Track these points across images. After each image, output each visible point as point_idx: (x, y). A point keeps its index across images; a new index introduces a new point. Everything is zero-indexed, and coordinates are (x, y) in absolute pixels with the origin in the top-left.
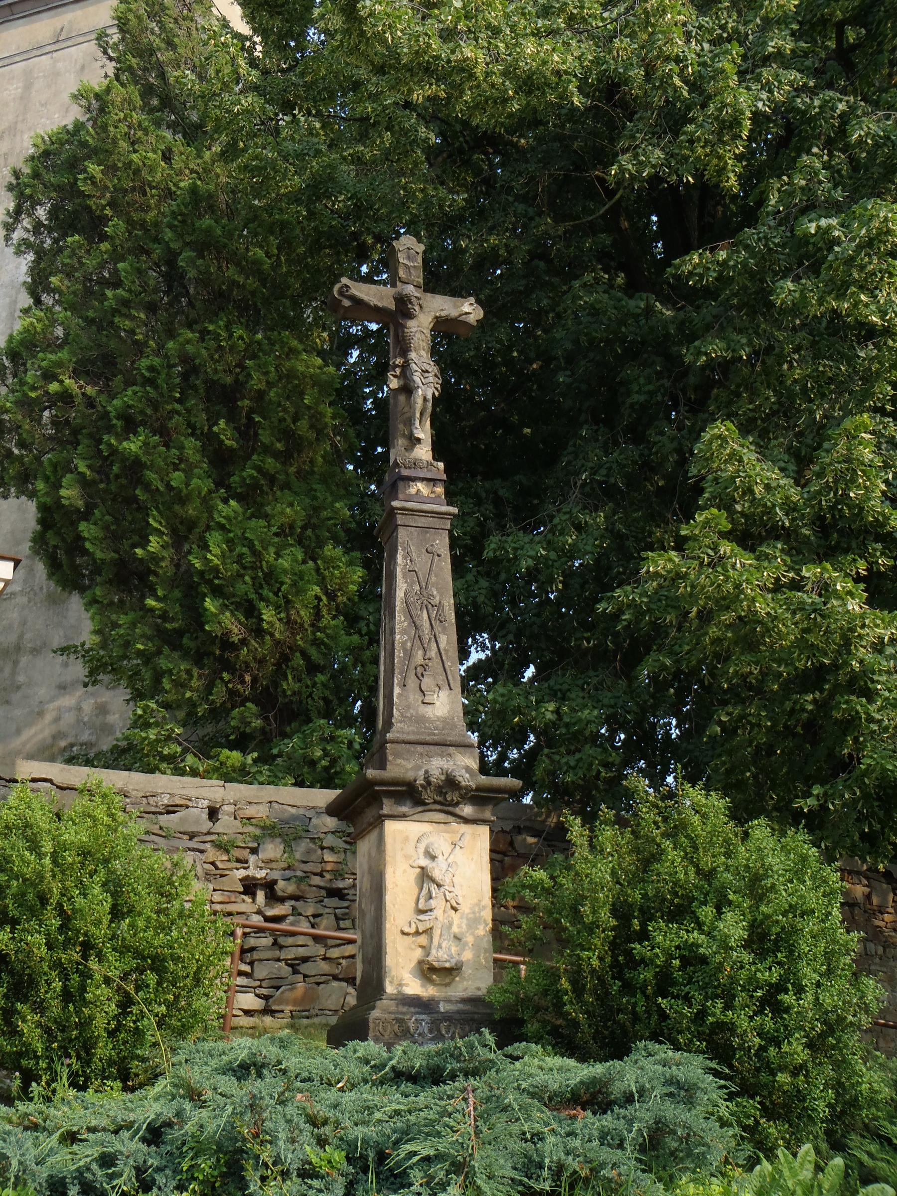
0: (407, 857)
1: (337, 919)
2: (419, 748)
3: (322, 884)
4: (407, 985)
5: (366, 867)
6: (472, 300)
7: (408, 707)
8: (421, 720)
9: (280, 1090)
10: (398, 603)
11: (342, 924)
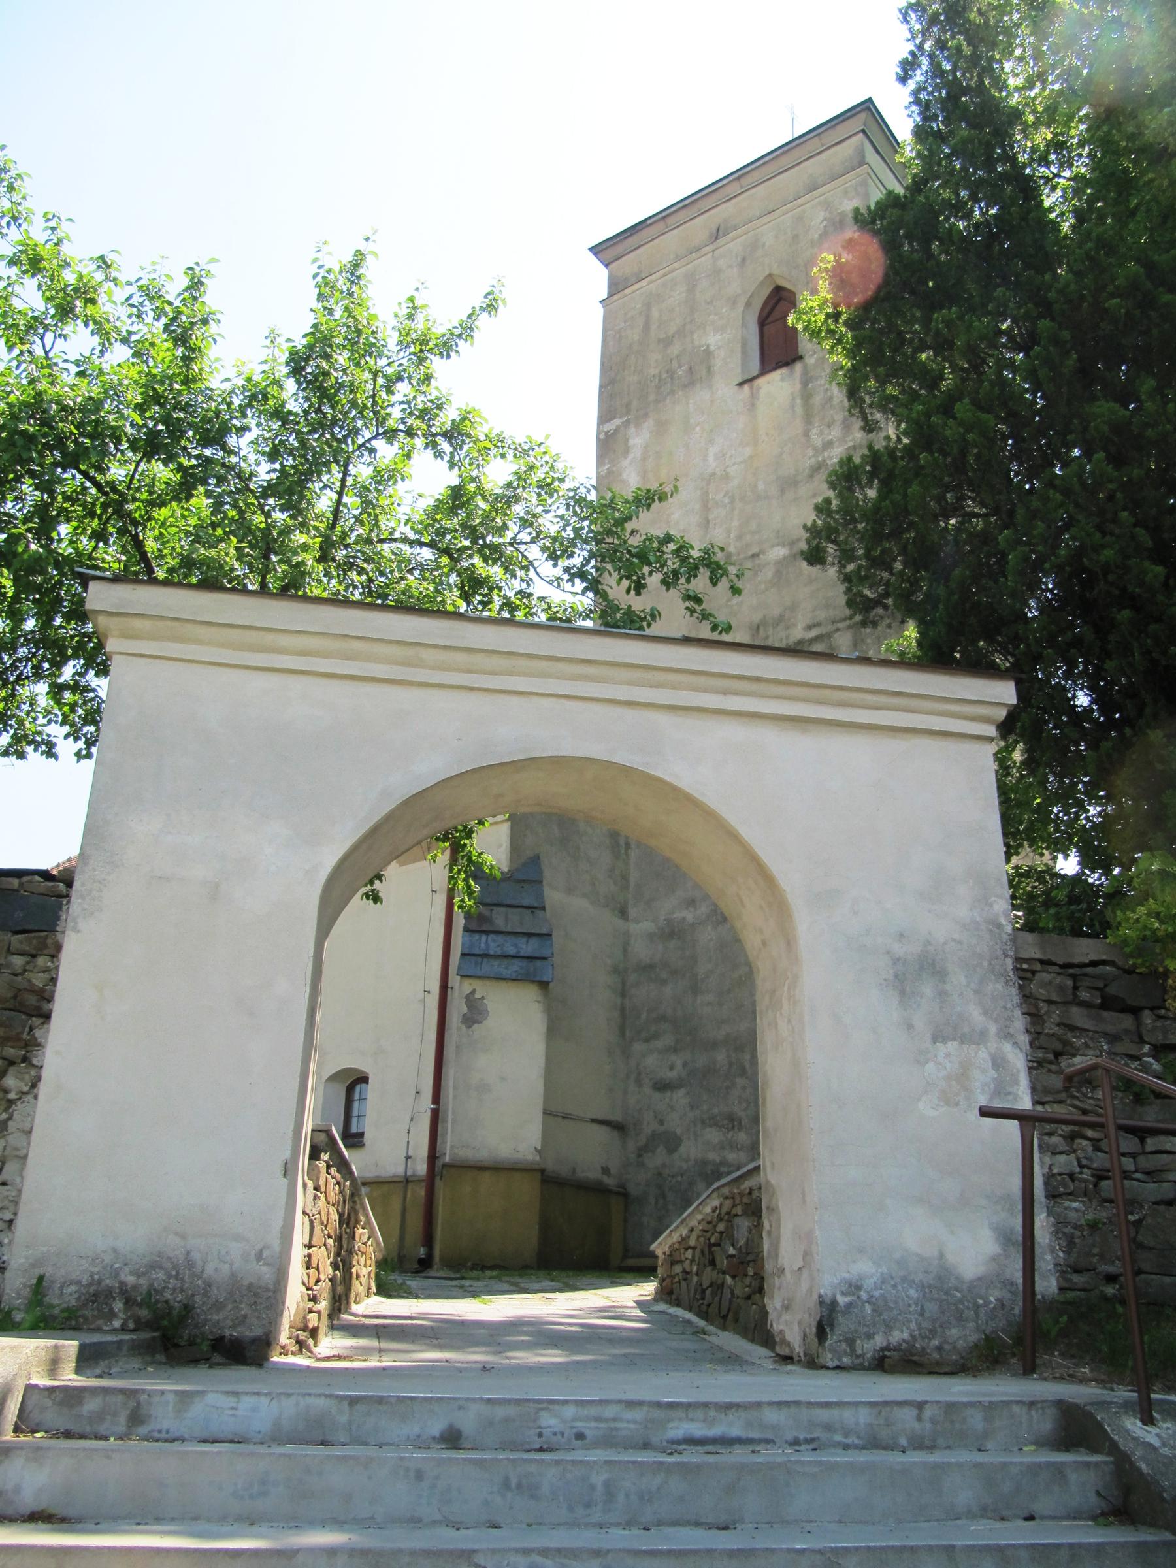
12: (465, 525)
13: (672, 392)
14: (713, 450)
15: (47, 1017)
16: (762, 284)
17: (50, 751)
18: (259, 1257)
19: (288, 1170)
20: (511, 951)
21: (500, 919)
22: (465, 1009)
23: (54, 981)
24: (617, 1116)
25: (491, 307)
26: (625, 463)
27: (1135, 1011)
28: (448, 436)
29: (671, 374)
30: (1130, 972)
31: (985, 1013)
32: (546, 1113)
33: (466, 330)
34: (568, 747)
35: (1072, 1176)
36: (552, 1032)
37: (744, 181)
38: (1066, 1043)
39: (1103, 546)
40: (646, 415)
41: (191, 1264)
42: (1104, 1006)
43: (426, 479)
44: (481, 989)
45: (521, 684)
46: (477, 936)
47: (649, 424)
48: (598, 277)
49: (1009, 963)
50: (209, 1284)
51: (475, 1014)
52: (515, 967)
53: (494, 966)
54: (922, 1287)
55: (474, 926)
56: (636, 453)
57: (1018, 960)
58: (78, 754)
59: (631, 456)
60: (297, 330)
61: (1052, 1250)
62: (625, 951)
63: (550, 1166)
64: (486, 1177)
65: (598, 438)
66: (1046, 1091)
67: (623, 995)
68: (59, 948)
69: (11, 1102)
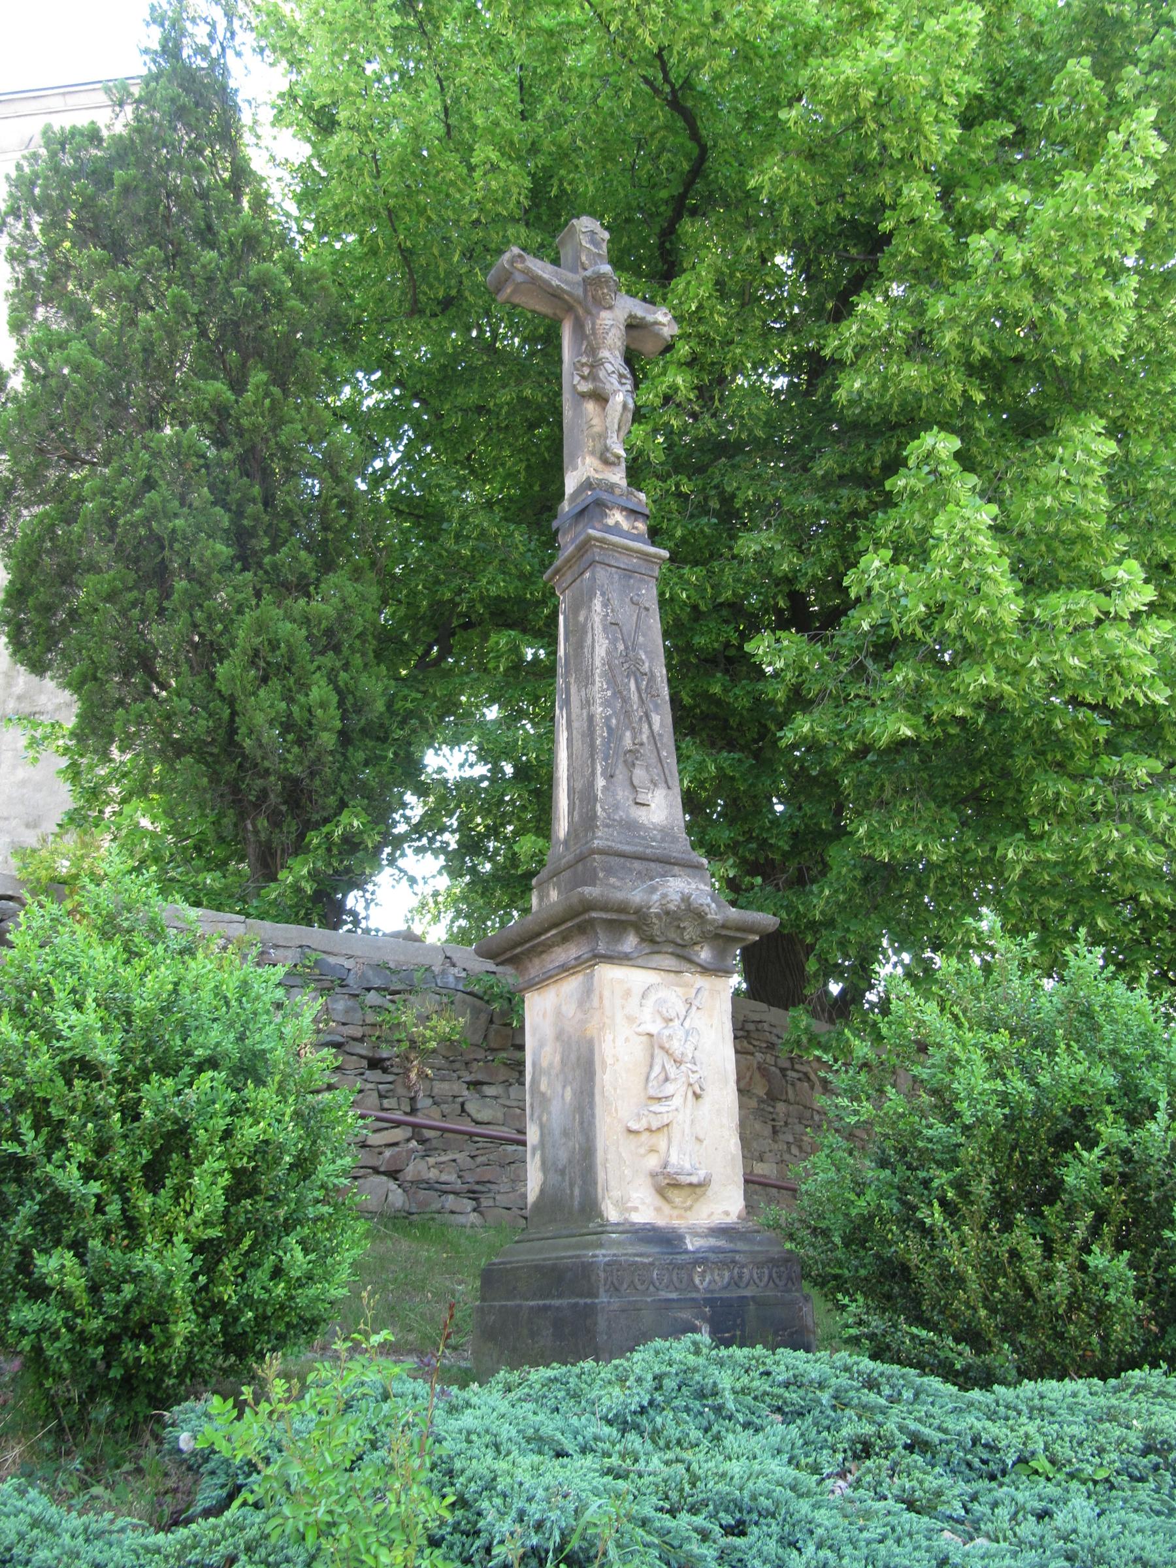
0: (630, 1019)
1: (381, 1096)
2: (637, 865)
3: (364, 1052)
4: (636, 1209)
7: (616, 807)
8: (631, 826)
9: (695, 1466)
10: (598, 663)
39: (176, 515)
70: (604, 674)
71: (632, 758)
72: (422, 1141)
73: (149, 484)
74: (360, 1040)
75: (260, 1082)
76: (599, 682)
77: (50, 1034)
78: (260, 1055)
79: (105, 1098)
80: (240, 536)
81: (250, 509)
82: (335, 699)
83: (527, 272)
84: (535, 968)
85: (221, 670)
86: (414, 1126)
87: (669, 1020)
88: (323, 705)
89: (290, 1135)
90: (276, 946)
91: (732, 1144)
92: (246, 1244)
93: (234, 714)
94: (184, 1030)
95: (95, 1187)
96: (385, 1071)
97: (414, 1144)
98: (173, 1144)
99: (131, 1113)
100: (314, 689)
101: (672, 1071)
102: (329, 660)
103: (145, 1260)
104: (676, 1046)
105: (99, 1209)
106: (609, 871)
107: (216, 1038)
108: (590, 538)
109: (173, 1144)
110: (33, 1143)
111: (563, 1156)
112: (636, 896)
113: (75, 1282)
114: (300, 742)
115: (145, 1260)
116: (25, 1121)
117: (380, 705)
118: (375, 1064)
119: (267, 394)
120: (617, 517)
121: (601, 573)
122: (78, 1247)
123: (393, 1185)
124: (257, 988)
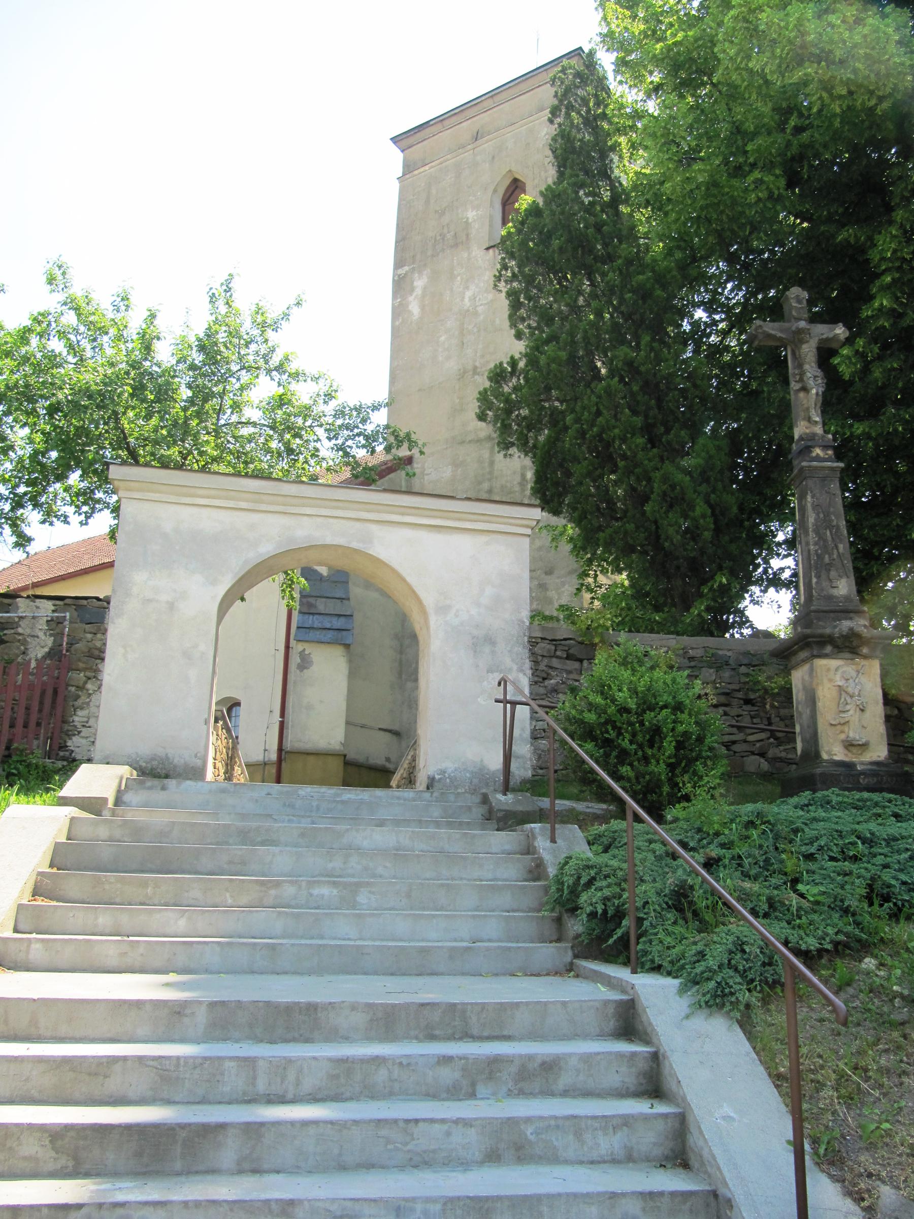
0: (830, 680)
1: (752, 717)
2: (832, 615)
5: (800, 687)
6: (841, 325)
7: (822, 590)
8: (830, 598)
10: (186, 513)
11: (755, 721)
12: (287, 422)
13: (443, 250)
14: (468, 294)
15: (103, 659)
16: (505, 176)
17: (66, 521)
18: (196, 756)
19: (207, 722)
20: (328, 626)
21: (321, 605)
22: (299, 660)
23: (105, 644)
24: (396, 727)
25: (298, 304)
26: (411, 298)
27: (581, 661)
28: (277, 369)
29: (443, 236)
30: (581, 643)
31: (513, 660)
32: (348, 723)
33: (286, 316)
34: (329, 540)
35: (544, 731)
36: (352, 675)
37: (496, 99)
38: (548, 674)
39: (614, 427)
40: (425, 265)
41: (167, 758)
42: (568, 658)
43: (265, 388)
44: (309, 648)
45: (308, 511)
46: (307, 616)
47: (427, 272)
48: (396, 158)
49: (526, 639)
50: (175, 767)
51: (305, 663)
52: (330, 635)
53: (318, 635)
54: (472, 772)
55: (305, 610)
56: (418, 291)
57: (530, 637)
58: (81, 523)
59: (415, 294)
60: (199, 330)
61: (531, 760)
62: (403, 625)
63: (351, 756)
64: (311, 759)
65: (394, 280)
66: (537, 694)
67: (401, 653)
68: (106, 630)
69: (90, 695)
70: (814, 531)
71: (829, 567)
72: (776, 739)
73: (599, 413)
74: (739, 691)
75: (682, 712)
76: (812, 535)
77: (613, 701)
78: (681, 703)
79: (633, 719)
80: (648, 429)
81: (651, 413)
82: (709, 512)
83: (764, 332)
84: (794, 660)
85: (647, 508)
86: (771, 731)
87: (847, 680)
88: (704, 516)
89: (694, 728)
90: (692, 648)
91: (881, 728)
92: (683, 764)
93: (657, 528)
94: (655, 696)
95: (634, 746)
96: (753, 705)
97: (772, 740)
98: (656, 733)
99: (642, 723)
100: (698, 508)
101: (849, 700)
102: (704, 488)
103: (652, 767)
104: (850, 690)
105: (636, 753)
106: (819, 619)
107: (666, 698)
108: (802, 468)
109: (656, 733)
110: (613, 734)
111: (808, 736)
112: (828, 631)
113: (631, 774)
114: (693, 539)
115: (652, 767)
116: (609, 727)
117: (735, 510)
118: (748, 702)
119: (652, 349)
120: (818, 451)
121: (810, 483)
122: (631, 765)
123: (762, 760)
124: (678, 680)
